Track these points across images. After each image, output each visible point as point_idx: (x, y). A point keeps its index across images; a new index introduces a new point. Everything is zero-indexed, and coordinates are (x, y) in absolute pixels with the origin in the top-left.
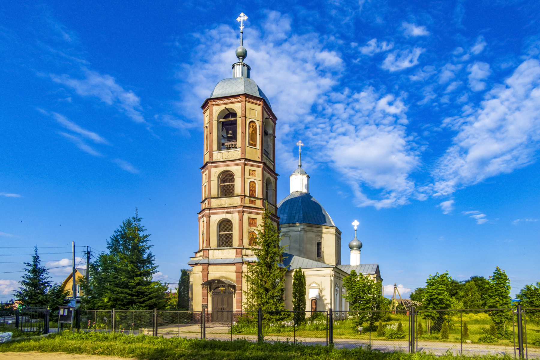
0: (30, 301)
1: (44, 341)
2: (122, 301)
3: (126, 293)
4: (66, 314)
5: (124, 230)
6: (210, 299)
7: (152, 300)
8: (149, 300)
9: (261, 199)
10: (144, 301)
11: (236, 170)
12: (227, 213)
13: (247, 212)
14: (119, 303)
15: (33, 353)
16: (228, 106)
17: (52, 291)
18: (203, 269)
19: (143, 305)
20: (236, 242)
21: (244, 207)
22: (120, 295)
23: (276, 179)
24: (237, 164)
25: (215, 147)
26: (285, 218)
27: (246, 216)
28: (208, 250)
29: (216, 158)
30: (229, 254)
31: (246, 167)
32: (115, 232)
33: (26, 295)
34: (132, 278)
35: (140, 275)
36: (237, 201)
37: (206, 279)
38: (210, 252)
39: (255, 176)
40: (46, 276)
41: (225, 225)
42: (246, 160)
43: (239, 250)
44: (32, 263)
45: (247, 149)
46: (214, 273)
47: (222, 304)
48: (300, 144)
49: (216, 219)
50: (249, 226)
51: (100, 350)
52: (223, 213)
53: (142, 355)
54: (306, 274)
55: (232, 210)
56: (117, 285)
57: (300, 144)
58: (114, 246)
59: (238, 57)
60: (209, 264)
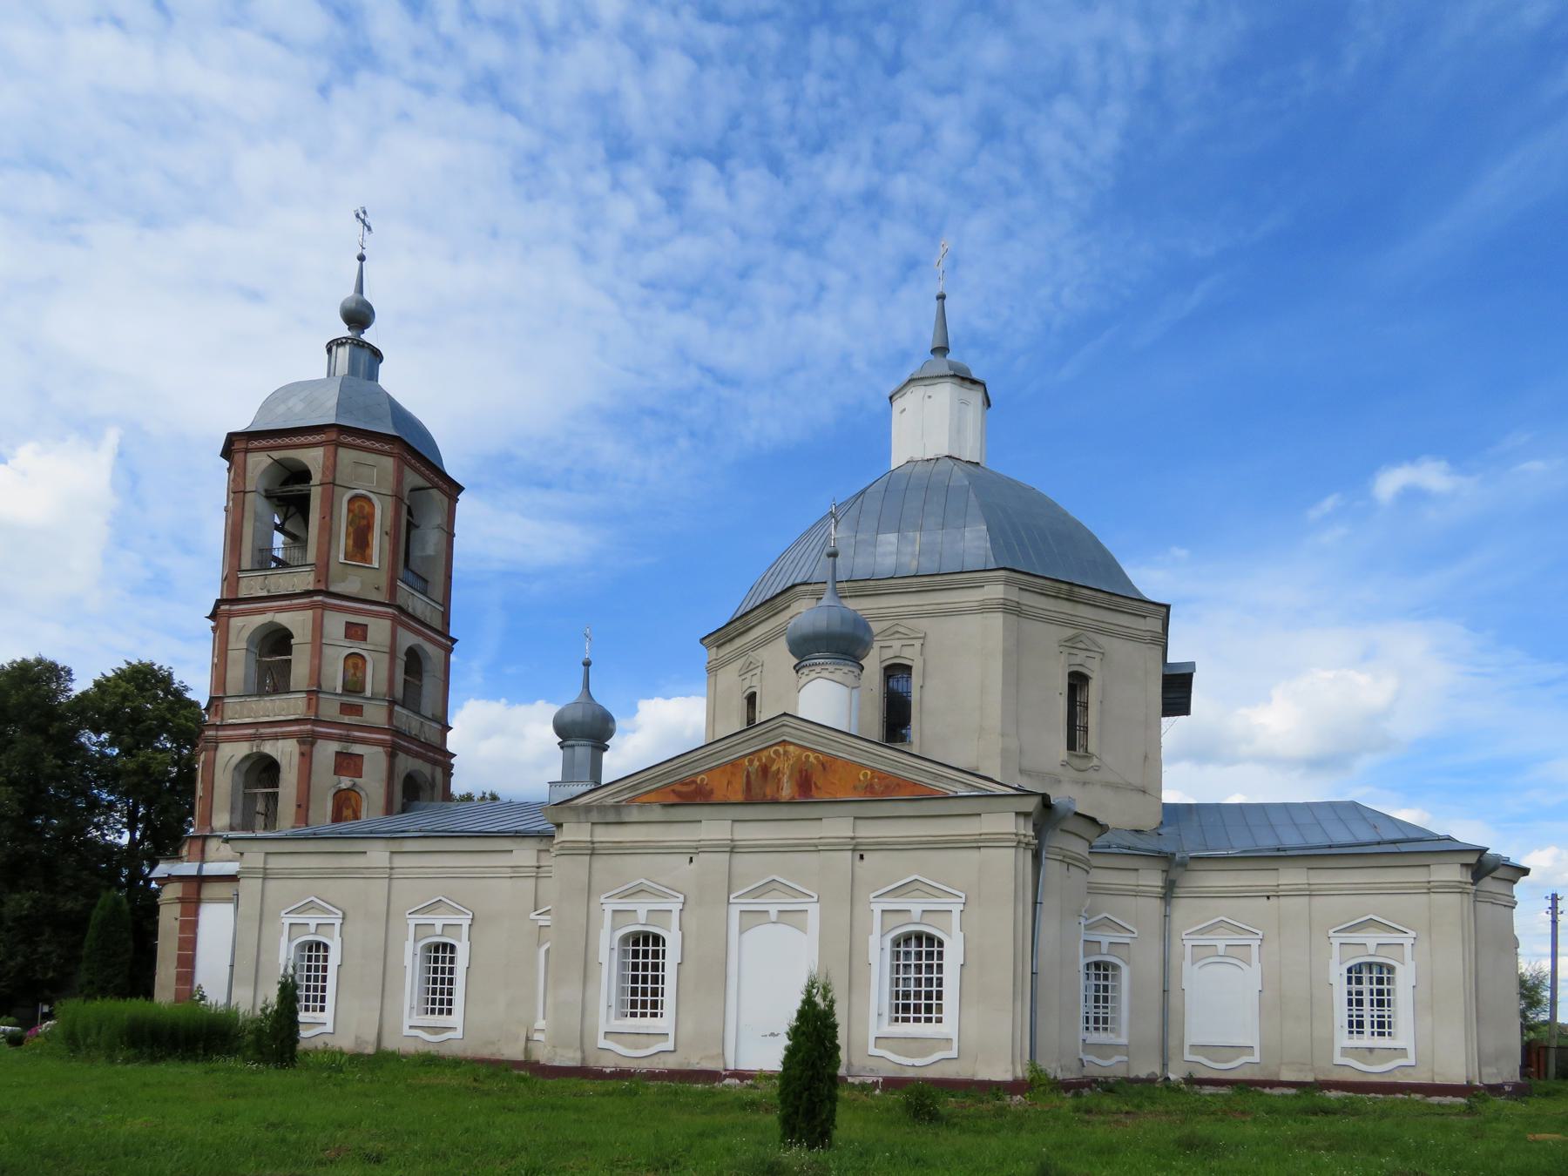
21: (317, 722)
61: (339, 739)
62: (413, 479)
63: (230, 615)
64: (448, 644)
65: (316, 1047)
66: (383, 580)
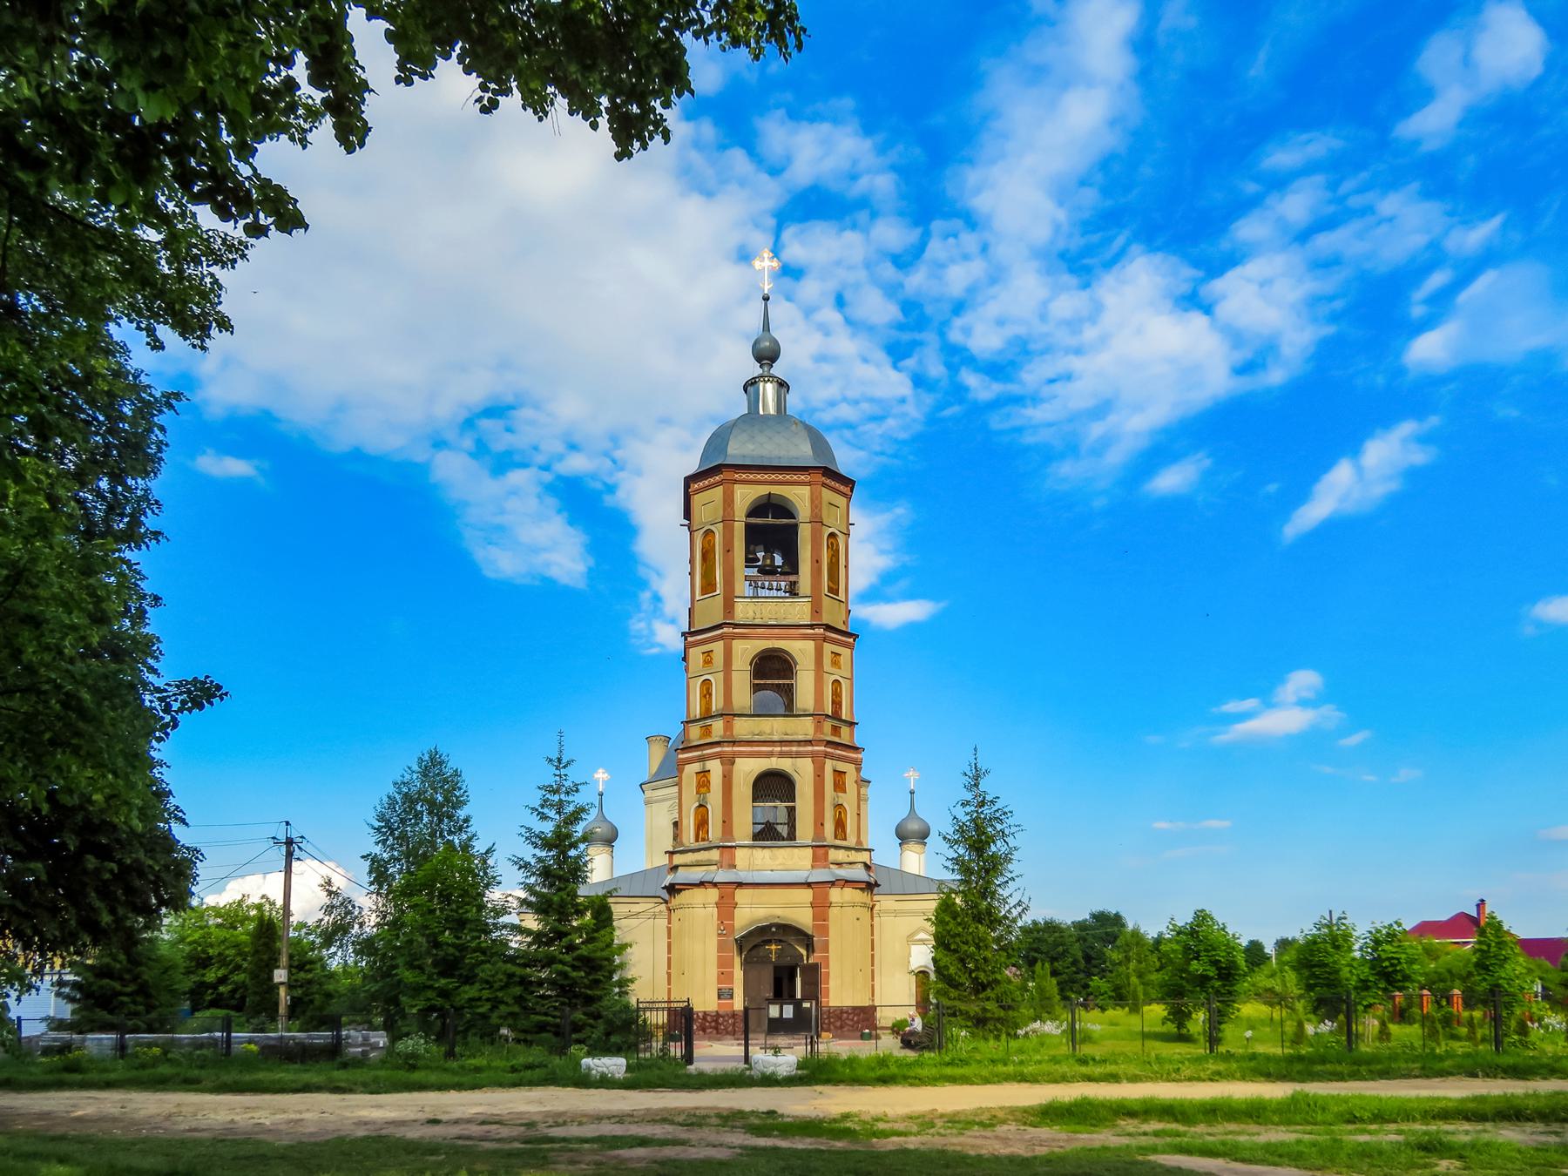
6: (738, 974)
12: (782, 755)
18: (722, 897)
24: (805, 637)
29: (741, 615)
36: (803, 728)
38: (739, 853)
39: (840, 668)
49: (749, 768)
50: (835, 791)
51: (613, 1120)
52: (769, 755)
54: (614, 908)
55: (794, 749)
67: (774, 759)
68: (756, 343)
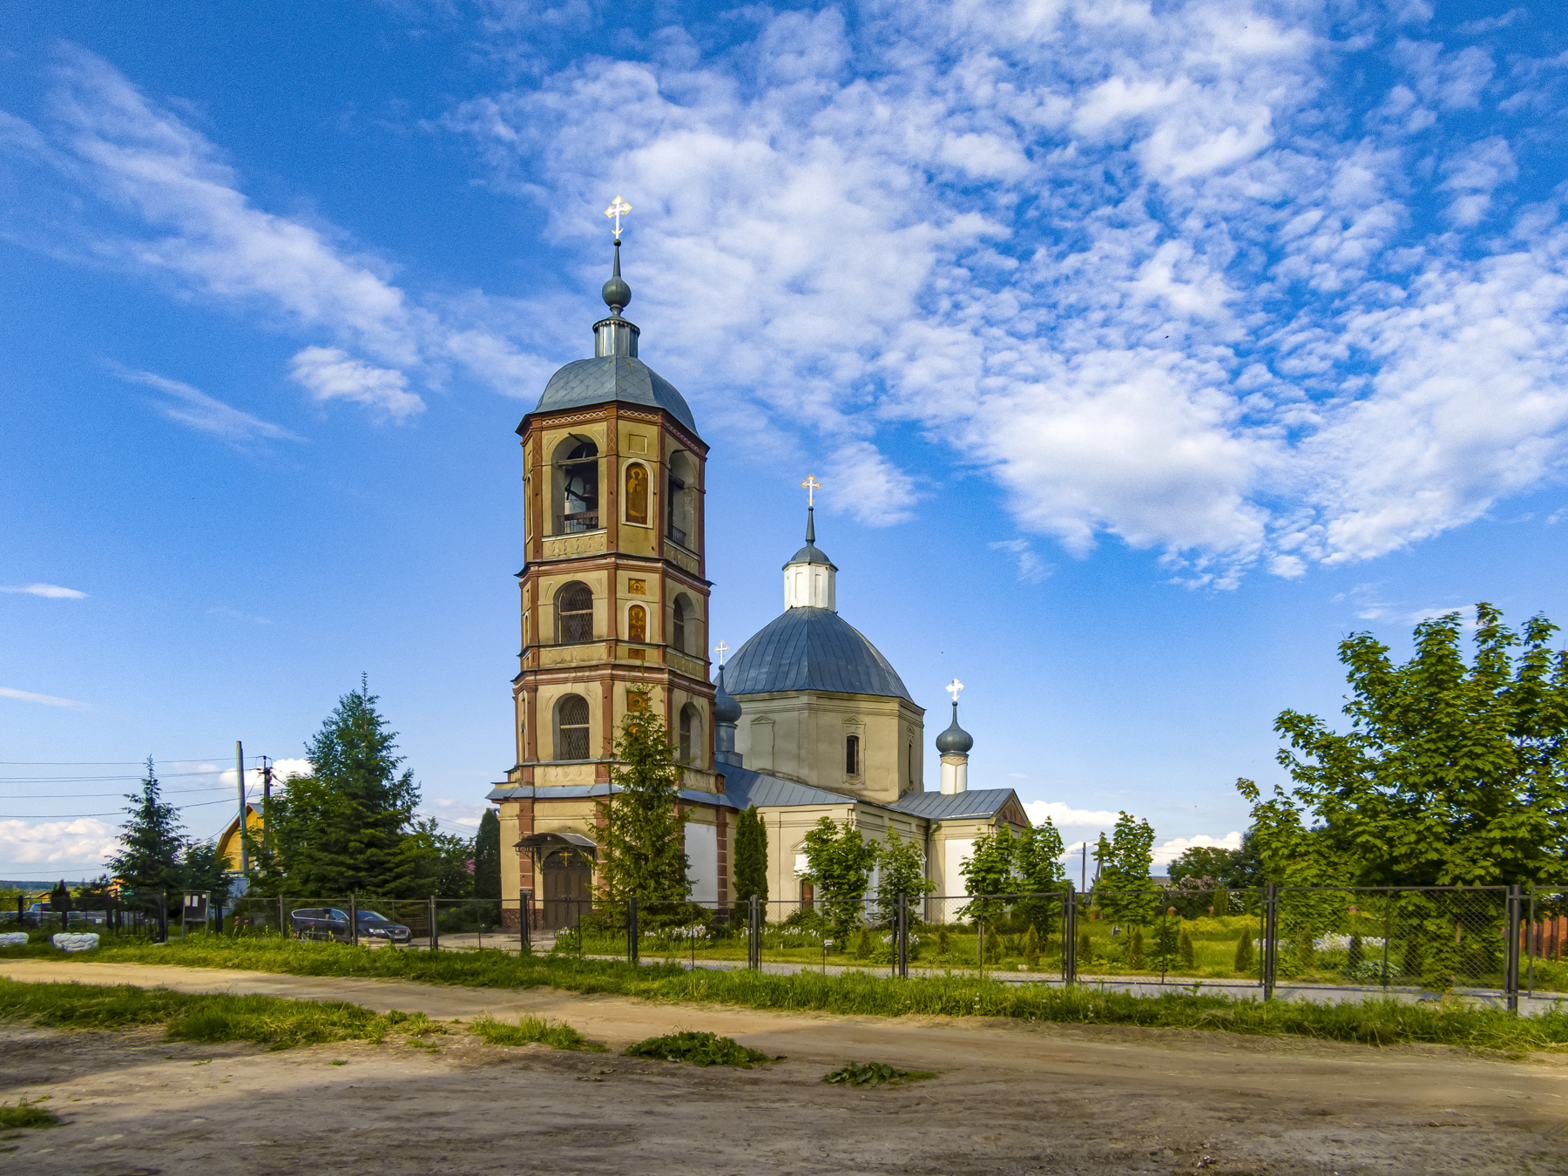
0: (141, 880)
1: (156, 948)
2: (335, 880)
3: (342, 864)
4: (195, 904)
5: (345, 721)
6: (539, 878)
7: (402, 880)
8: (395, 878)
9: (659, 646)
10: (386, 882)
11: (596, 579)
12: (576, 680)
13: (623, 679)
14: (328, 885)
15: (130, 965)
16: (576, 430)
17: (192, 857)
18: (521, 810)
19: (380, 890)
20: (596, 749)
21: (615, 667)
22: (329, 868)
23: (707, 594)
24: (599, 568)
25: (548, 527)
26: (763, 677)
27: (619, 688)
28: (533, 766)
30: (581, 777)
31: (619, 572)
32: (325, 724)
33: (133, 867)
34: (354, 830)
35: (375, 825)
36: (598, 653)
37: (528, 833)
40: (175, 823)
41: (573, 707)
42: (619, 556)
43: (601, 768)
44: (144, 796)
45: (623, 531)
46: (548, 820)
47: (568, 890)
48: (811, 485)
52: (565, 681)
53: (893, 1169)
55: (587, 674)
56: (325, 847)
57: (811, 485)
58: (323, 757)
59: (609, 303)
60: (535, 800)
61: (687, 690)
62: (672, 444)
63: (539, 575)
64: (704, 586)
65: (1091, 551)
66: (653, 541)
67: (569, 685)
68: (605, 287)
